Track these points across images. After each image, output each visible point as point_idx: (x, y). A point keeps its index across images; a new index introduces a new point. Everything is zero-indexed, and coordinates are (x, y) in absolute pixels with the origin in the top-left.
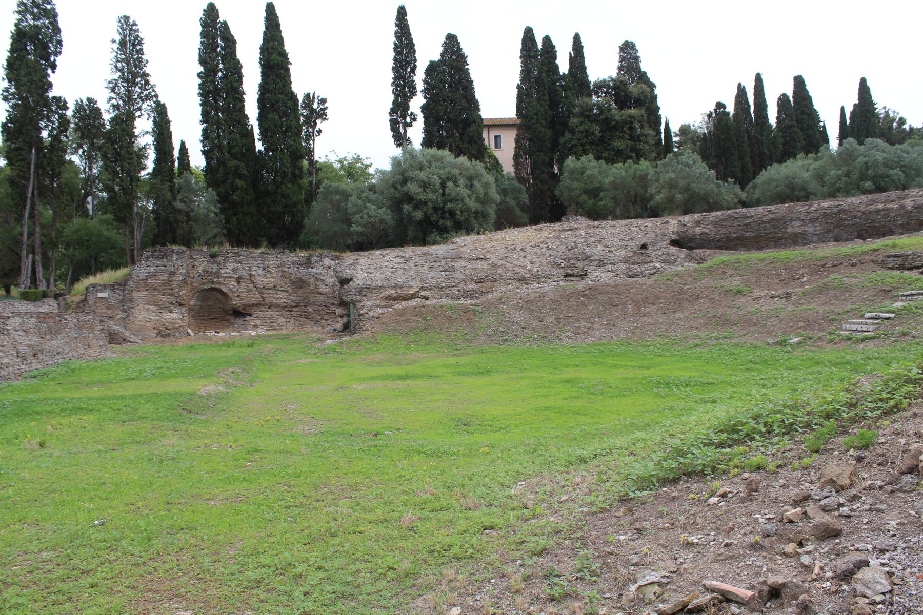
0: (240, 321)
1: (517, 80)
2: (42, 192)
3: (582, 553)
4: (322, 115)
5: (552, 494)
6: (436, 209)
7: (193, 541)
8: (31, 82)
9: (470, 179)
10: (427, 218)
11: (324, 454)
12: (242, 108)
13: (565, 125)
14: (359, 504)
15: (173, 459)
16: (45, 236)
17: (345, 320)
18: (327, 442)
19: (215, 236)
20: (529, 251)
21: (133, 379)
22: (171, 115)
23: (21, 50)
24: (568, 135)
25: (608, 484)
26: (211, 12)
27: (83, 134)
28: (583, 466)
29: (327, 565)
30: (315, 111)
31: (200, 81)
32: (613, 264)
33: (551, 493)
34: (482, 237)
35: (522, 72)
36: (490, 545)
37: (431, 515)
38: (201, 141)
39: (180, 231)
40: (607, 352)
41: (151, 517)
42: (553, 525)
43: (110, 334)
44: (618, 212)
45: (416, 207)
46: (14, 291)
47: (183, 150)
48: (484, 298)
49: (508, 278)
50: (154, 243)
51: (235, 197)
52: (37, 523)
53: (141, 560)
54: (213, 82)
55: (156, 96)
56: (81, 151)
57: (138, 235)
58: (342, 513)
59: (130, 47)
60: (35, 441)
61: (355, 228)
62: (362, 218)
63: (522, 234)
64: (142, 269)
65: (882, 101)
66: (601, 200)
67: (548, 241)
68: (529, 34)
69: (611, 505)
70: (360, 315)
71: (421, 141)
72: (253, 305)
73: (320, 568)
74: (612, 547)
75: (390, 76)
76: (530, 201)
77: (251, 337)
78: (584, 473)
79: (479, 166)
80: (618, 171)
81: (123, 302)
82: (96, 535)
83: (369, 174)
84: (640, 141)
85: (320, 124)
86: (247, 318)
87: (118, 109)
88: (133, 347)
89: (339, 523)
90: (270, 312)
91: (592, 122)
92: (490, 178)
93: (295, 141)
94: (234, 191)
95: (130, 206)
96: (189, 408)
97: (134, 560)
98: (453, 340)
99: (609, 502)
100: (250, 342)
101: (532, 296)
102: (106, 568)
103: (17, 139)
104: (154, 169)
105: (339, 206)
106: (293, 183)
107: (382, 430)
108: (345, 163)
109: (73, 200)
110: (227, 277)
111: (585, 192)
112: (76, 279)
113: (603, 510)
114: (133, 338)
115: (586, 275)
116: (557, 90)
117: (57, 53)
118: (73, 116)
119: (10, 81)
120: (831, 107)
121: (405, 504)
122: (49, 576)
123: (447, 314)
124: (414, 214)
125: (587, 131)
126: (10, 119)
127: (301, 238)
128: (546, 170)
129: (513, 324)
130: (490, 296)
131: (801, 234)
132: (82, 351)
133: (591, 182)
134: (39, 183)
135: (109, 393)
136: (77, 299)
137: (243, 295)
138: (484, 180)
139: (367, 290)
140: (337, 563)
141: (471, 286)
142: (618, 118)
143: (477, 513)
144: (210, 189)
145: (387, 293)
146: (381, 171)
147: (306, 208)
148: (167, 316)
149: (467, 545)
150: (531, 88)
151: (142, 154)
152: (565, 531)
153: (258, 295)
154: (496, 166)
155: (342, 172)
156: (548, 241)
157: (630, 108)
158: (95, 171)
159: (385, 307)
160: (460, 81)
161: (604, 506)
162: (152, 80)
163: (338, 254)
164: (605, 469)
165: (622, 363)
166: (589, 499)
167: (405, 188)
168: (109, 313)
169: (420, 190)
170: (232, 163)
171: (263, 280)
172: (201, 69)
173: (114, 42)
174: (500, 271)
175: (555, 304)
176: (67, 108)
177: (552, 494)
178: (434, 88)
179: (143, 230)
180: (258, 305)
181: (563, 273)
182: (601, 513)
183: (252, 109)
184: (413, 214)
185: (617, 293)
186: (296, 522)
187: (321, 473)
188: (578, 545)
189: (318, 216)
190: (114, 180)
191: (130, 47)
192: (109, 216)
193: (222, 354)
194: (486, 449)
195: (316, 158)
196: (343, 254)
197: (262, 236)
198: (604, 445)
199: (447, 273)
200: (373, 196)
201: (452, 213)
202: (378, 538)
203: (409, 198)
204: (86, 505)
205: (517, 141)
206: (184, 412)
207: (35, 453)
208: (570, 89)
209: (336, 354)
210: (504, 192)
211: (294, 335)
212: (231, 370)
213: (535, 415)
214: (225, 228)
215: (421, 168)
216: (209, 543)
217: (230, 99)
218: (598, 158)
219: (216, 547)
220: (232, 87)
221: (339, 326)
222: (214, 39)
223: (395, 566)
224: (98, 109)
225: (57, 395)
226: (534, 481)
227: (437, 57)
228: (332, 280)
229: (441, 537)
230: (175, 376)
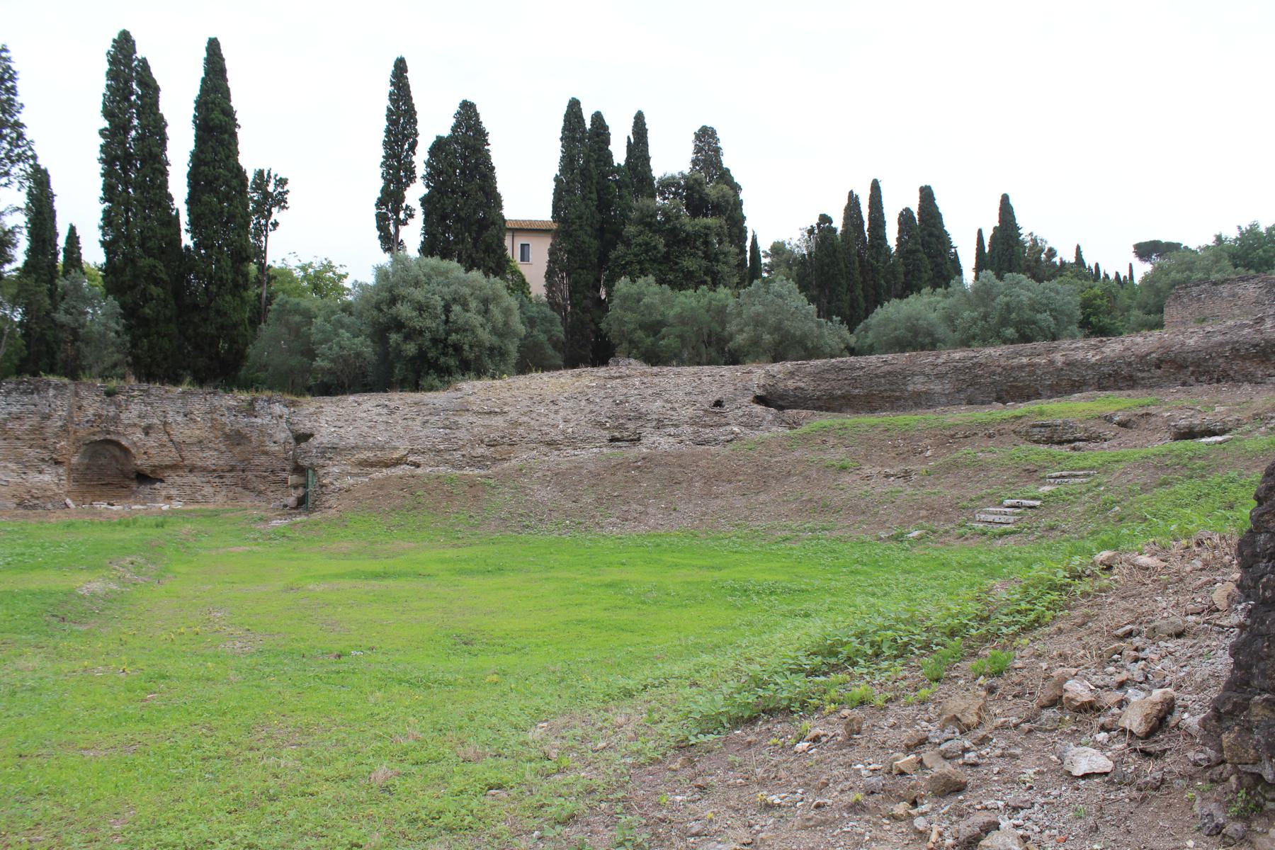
0: (146, 489)
1: (555, 170)
4: (280, 201)
5: (584, 740)
6: (435, 341)
9: (485, 301)
11: (263, 683)
12: (164, 185)
13: (618, 234)
15: (33, 689)
17: (300, 492)
18: (268, 665)
22: (55, 186)
24: (621, 248)
25: (661, 726)
26: (124, 44)
28: (628, 702)
30: (271, 196)
31: (102, 141)
32: (676, 426)
33: (583, 738)
34: (497, 383)
36: (497, 811)
37: (414, 769)
38: (101, 228)
39: (61, 356)
42: (585, 781)
45: (407, 338)
47: (73, 238)
49: (532, 441)
50: (19, 371)
51: (147, 310)
54: (123, 143)
55: (34, 157)
61: (319, 363)
62: (330, 349)
63: (553, 380)
69: (664, 755)
70: (322, 486)
71: (418, 246)
72: (167, 467)
74: (664, 812)
77: (162, 513)
78: (629, 710)
79: (497, 283)
80: (688, 300)
83: (344, 289)
84: (718, 261)
85: (276, 214)
86: (158, 485)
89: (280, 781)
90: (191, 478)
91: (655, 232)
92: (512, 302)
93: (239, 235)
94: (146, 301)
96: (62, 614)
99: (662, 750)
100: (160, 519)
101: (564, 467)
104: (26, 263)
106: (234, 296)
110: (129, 425)
111: (642, 326)
113: (654, 761)
115: (639, 439)
116: (609, 187)
121: (377, 753)
123: (446, 487)
124: (404, 347)
125: (647, 244)
127: (242, 373)
128: (589, 294)
129: (537, 504)
130: (506, 465)
131: (926, 393)
133: (650, 314)
137: (152, 451)
138: (504, 305)
141: (480, 451)
142: (689, 228)
143: (479, 767)
144: (111, 298)
145: (362, 456)
146: (361, 285)
148: (34, 478)
149: (464, 811)
150: (573, 181)
152: (601, 790)
153: (174, 454)
154: (521, 285)
155: (305, 284)
157: (706, 215)
159: (357, 475)
160: (477, 166)
161: (655, 755)
162: (29, 134)
163: (295, 398)
166: (634, 746)
167: (394, 311)
169: (414, 314)
170: (146, 262)
171: (182, 431)
172: (106, 124)
174: (521, 430)
177: (584, 740)
178: (440, 173)
180: (174, 467)
181: (608, 437)
182: (650, 764)
183: (178, 187)
184: (403, 347)
185: (680, 466)
186: (217, 780)
187: (257, 710)
188: (619, 808)
189: (267, 344)
193: (117, 536)
196: (301, 399)
197: (184, 369)
198: (658, 673)
199: (448, 431)
200: (347, 319)
201: (458, 348)
202: (338, 802)
203: (398, 325)
205: (552, 253)
206: (55, 621)
208: (627, 187)
209: (285, 541)
210: (530, 322)
211: (225, 512)
212: (129, 559)
214: (130, 354)
215: (417, 284)
216: (81, 815)
217: (147, 170)
218: (660, 281)
221: (291, 501)
223: (360, 842)
226: (560, 721)
227: (446, 132)
228: (283, 435)
229: (428, 801)
230: (42, 567)
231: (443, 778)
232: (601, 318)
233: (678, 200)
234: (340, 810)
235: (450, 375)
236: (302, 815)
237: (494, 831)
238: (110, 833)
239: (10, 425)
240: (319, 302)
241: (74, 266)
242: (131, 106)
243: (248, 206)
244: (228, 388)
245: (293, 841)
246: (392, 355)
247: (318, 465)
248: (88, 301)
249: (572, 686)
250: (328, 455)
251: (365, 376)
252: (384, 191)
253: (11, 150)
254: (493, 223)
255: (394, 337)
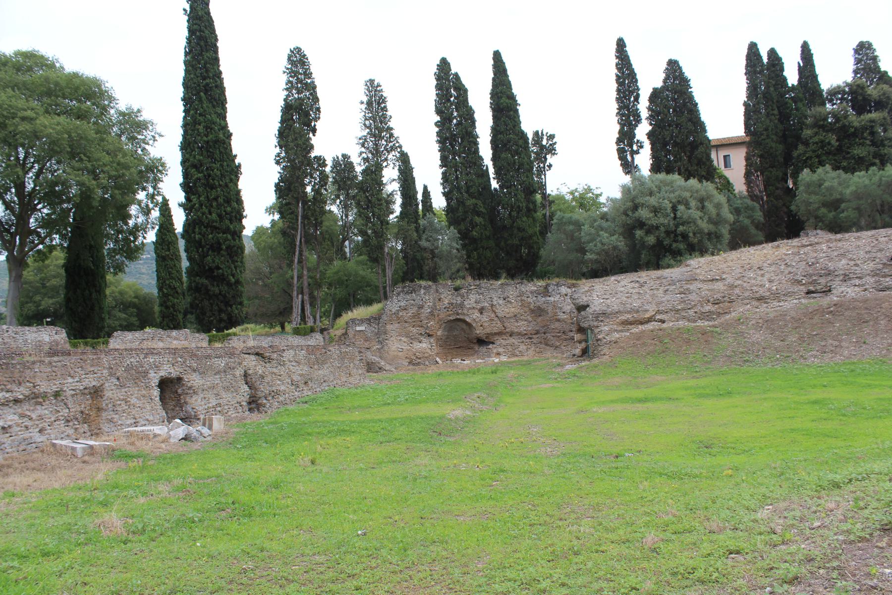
0: (483, 349)
1: (743, 97)
2: (308, 239)
3: (839, 584)
4: (552, 150)
5: (802, 520)
6: (668, 233)
7: (444, 553)
8: (297, 146)
9: (702, 200)
10: (659, 242)
11: (566, 475)
12: (477, 151)
13: (798, 138)
14: (600, 524)
15: (426, 477)
16: (311, 277)
17: (583, 345)
18: (569, 463)
19: (458, 271)
20: (767, 269)
21: (389, 404)
22: (413, 163)
23: (289, 120)
24: (801, 148)
25: (867, 511)
26: (444, 65)
27: (339, 186)
28: (837, 491)
29: (570, 582)
30: (545, 147)
31: (437, 129)
32: (860, 278)
33: (801, 518)
34: (716, 258)
35: (748, 89)
36: (736, 570)
37: (674, 537)
38: (442, 184)
39: (426, 268)
40: (858, 371)
41: (407, 530)
42: (805, 552)
43: (368, 364)
44: (863, 223)
45: (648, 232)
46: (288, 327)
47: (426, 193)
48: (722, 319)
49: (746, 298)
50: (403, 280)
51: (475, 233)
52: (310, 530)
53: (398, 569)
54: (449, 129)
55: (400, 147)
56: (338, 201)
57: (389, 273)
58: (584, 532)
59: (376, 105)
60: (307, 459)
61: (589, 256)
62: (595, 246)
63: (758, 252)
64: (394, 304)
66: (843, 212)
67: (786, 257)
68: (753, 49)
69: (871, 535)
70: (597, 340)
71: (649, 167)
72: (496, 334)
73: (563, 585)
74: (875, 581)
75: (614, 106)
76: (765, 218)
77: (494, 364)
78: (838, 498)
79: (709, 186)
80: (860, 179)
81: (378, 334)
82: (360, 543)
83: (600, 204)
84: (884, 146)
85: (550, 159)
86: (491, 346)
87: (368, 162)
88: (388, 375)
89: (581, 542)
90: (512, 340)
91: (827, 131)
92: (721, 198)
93: (527, 177)
94: (473, 228)
95: (381, 247)
96: (440, 430)
97: (392, 568)
98: (691, 362)
99: (868, 531)
100: (494, 368)
101: (772, 315)
102: (368, 573)
103: (287, 196)
104: (401, 213)
105: (572, 236)
106: (528, 217)
107: (623, 452)
108: (576, 194)
109: (333, 245)
110: (470, 308)
111: (825, 204)
112: (338, 315)
113: (862, 539)
114: (388, 367)
115: (830, 291)
116: (786, 103)
117: (317, 119)
118: (331, 171)
119: (281, 147)
121: (647, 525)
122: (322, 577)
123: (685, 336)
124: (646, 239)
125: (822, 142)
126: (281, 180)
127: (538, 268)
128: (780, 186)
129: (753, 344)
130: (728, 317)
132: (344, 379)
133: (831, 195)
134: (305, 232)
135: (368, 416)
136: (339, 333)
137: (486, 324)
138: (716, 201)
139: (603, 315)
140: (580, 581)
141: (708, 308)
142: (856, 124)
143: (721, 537)
144: (452, 228)
145: (623, 318)
146: (612, 200)
147: (541, 240)
148: (417, 346)
149: (711, 569)
150: (758, 103)
151: (389, 201)
152: (819, 559)
153: (499, 325)
154: (726, 186)
155: (574, 203)
156: (786, 257)
157: (870, 112)
158: (350, 218)
159: (622, 331)
160: (685, 104)
161: (863, 534)
162: (396, 133)
163: (574, 282)
164: (862, 495)
165: (877, 383)
166: (844, 527)
167: (637, 214)
168: (367, 344)
169: (651, 215)
170: (470, 202)
171: (504, 310)
172: (438, 118)
173: (362, 103)
174: (737, 291)
175: (798, 323)
176: (326, 165)
177: (802, 520)
178: (658, 113)
179: (393, 268)
180: (500, 334)
181: (805, 290)
182: (859, 542)
183: (486, 151)
184: (646, 240)
185: (866, 309)
186: (539, 539)
187: (564, 493)
188: (835, 574)
189: (552, 247)
190: (367, 225)
191: (376, 105)
192: (364, 258)
193: (468, 380)
194: (730, 472)
195: (549, 192)
196: (579, 282)
197: (501, 269)
198: (860, 470)
199: (683, 296)
200: (605, 224)
201: (685, 236)
202: (620, 558)
203: (641, 224)
204: (351, 516)
205: (747, 159)
206: (435, 435)
207: (309, 469)
208: (801, 101)
209: (576, 378)
210: (737, 211)
211: (535, 361)
212: (476, 395)
213: (781, 438)
214: (467, 262)
215: (651, 194)
216: (459, 556)
217: (466, 143)
218: (836, 168)
219: (464, 560)
220: (466, 132)
221: (578, 351)
222: (448, 90)
223: (638, 586)
224: (352, 163)
225: (325, 418)
226: (783, 505)
227: (659, 84)
228: (569, 307)
229: (685, 560)
230: (426, 401)
231: (695, 544)
232: (791, 202)
233: (845, 104)
234: (622, 563)
235: (681, 255)
236: (596, 565)
237: (735, 585)
238: (476, 569)
239: (401, 314)
240: (585, 215)
241: (428, 211)
242: (452, 104)
243: (530, 156)
244: (530, 278)
245: (591, 583)
246: (638, 247)
247: (594, 326)
248: (437, 231)
249: (790, 479)
250: (600, 319)
251: (621, 262)
252: (621, 132)
253: (387, 145)
254: (702, 144)
255: (639, 233)
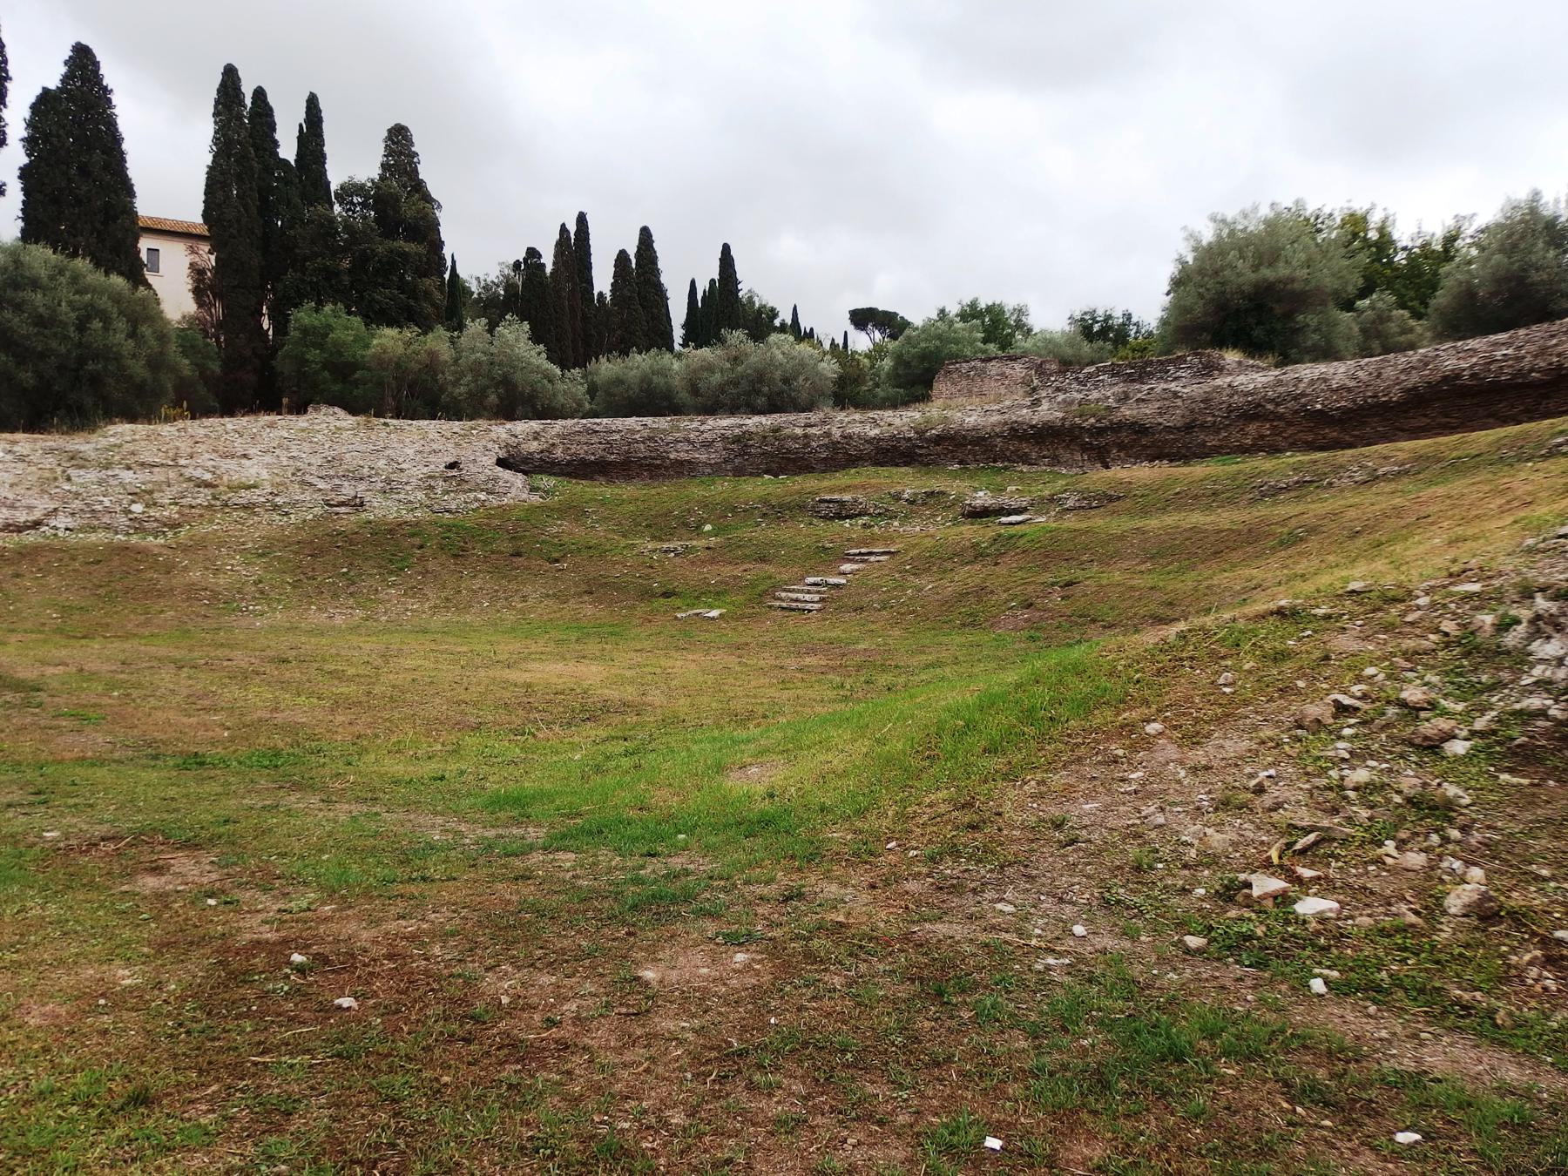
65: (753, 283)
68: (230, 74)
80: (389, 339)
120: (683, 274)
131: (689, 462)
227: (53, 83)
